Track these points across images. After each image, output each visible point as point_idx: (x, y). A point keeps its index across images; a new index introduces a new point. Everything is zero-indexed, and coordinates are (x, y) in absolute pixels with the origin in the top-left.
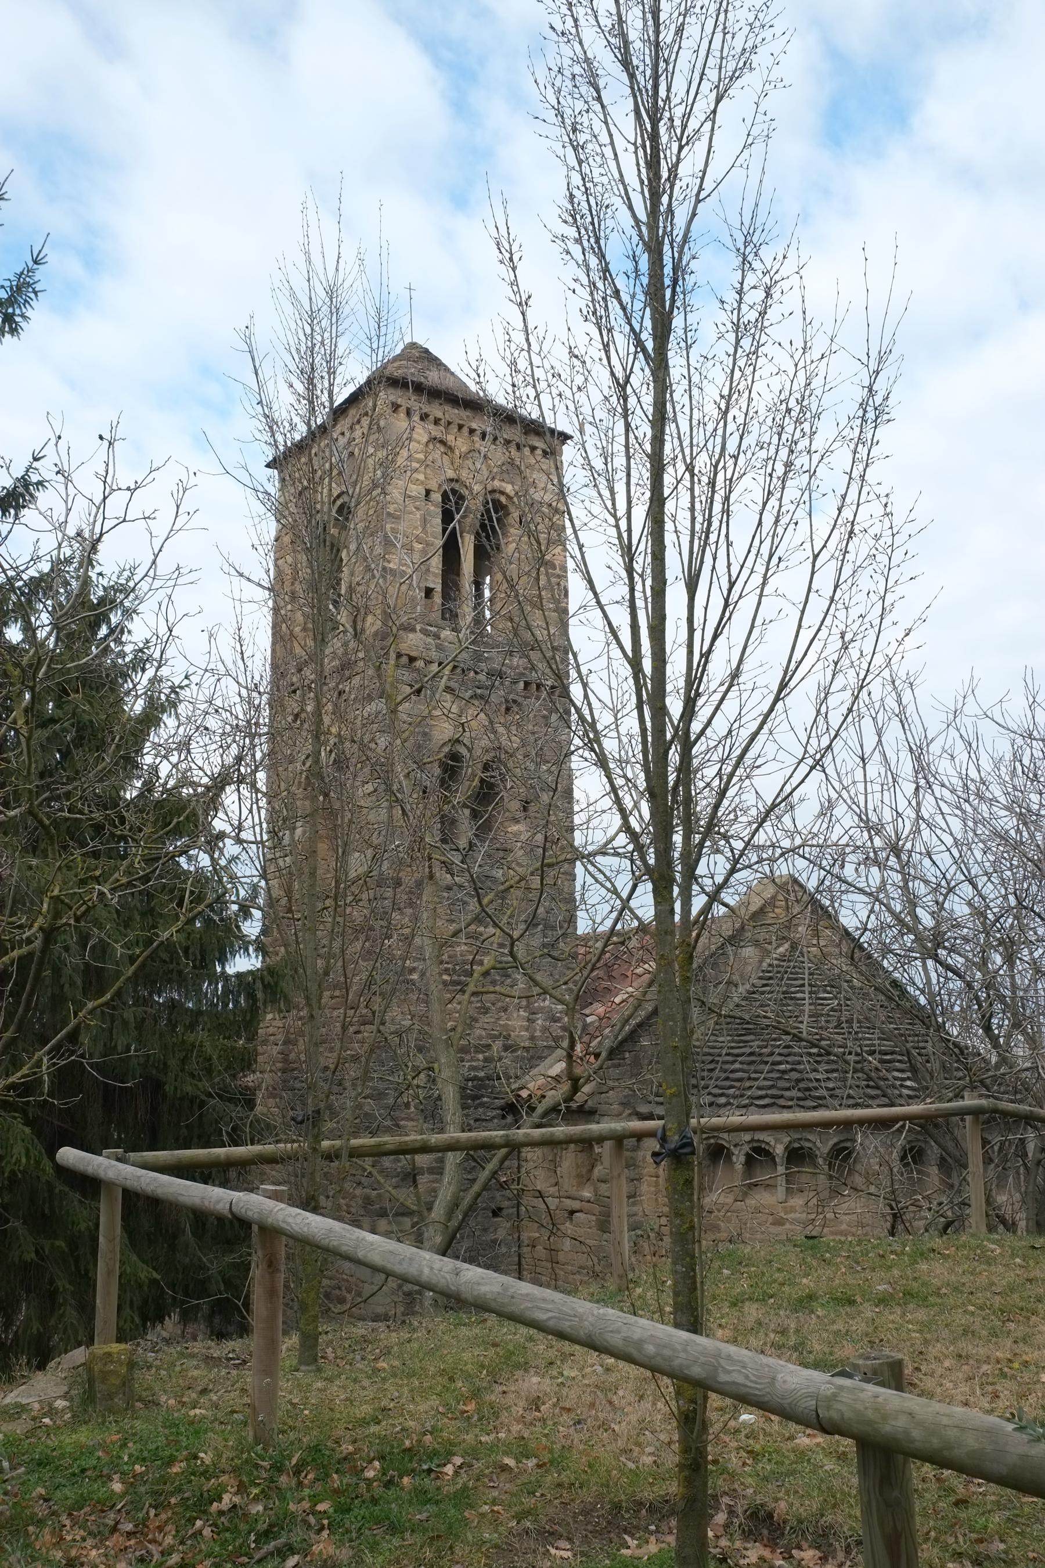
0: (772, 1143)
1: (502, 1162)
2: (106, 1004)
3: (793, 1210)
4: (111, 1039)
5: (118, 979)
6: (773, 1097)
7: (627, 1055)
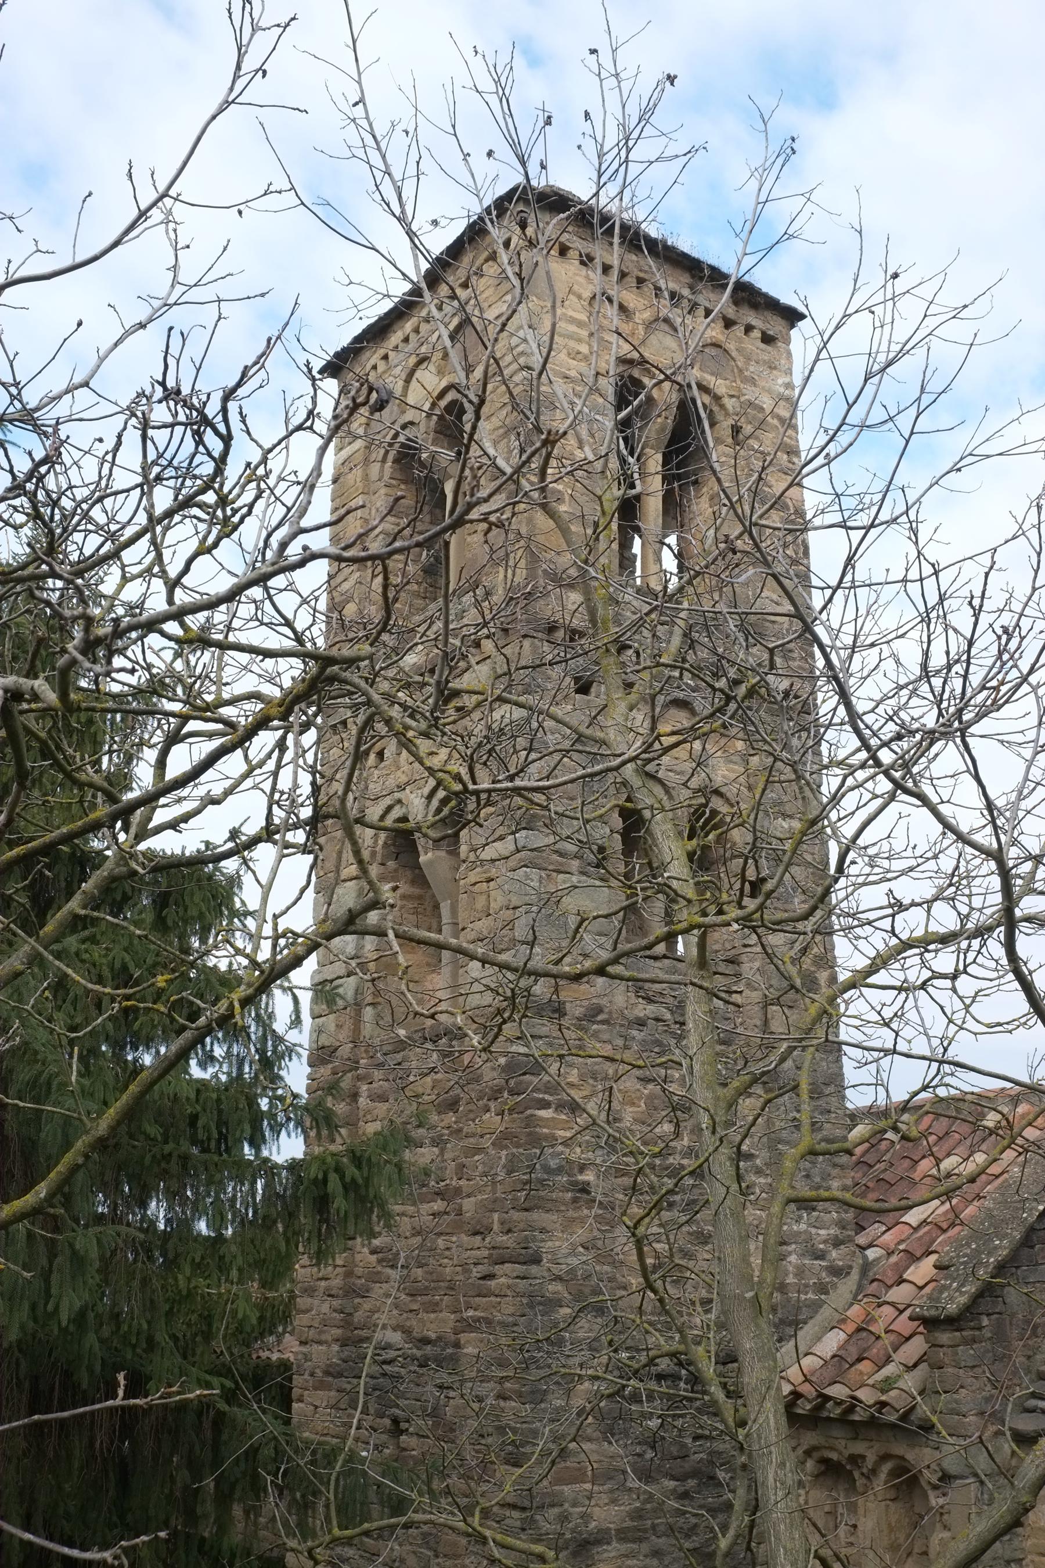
2: (34, 1213)
4: (48, 1295)
5: (67, 1146)
7: (985, 1321)
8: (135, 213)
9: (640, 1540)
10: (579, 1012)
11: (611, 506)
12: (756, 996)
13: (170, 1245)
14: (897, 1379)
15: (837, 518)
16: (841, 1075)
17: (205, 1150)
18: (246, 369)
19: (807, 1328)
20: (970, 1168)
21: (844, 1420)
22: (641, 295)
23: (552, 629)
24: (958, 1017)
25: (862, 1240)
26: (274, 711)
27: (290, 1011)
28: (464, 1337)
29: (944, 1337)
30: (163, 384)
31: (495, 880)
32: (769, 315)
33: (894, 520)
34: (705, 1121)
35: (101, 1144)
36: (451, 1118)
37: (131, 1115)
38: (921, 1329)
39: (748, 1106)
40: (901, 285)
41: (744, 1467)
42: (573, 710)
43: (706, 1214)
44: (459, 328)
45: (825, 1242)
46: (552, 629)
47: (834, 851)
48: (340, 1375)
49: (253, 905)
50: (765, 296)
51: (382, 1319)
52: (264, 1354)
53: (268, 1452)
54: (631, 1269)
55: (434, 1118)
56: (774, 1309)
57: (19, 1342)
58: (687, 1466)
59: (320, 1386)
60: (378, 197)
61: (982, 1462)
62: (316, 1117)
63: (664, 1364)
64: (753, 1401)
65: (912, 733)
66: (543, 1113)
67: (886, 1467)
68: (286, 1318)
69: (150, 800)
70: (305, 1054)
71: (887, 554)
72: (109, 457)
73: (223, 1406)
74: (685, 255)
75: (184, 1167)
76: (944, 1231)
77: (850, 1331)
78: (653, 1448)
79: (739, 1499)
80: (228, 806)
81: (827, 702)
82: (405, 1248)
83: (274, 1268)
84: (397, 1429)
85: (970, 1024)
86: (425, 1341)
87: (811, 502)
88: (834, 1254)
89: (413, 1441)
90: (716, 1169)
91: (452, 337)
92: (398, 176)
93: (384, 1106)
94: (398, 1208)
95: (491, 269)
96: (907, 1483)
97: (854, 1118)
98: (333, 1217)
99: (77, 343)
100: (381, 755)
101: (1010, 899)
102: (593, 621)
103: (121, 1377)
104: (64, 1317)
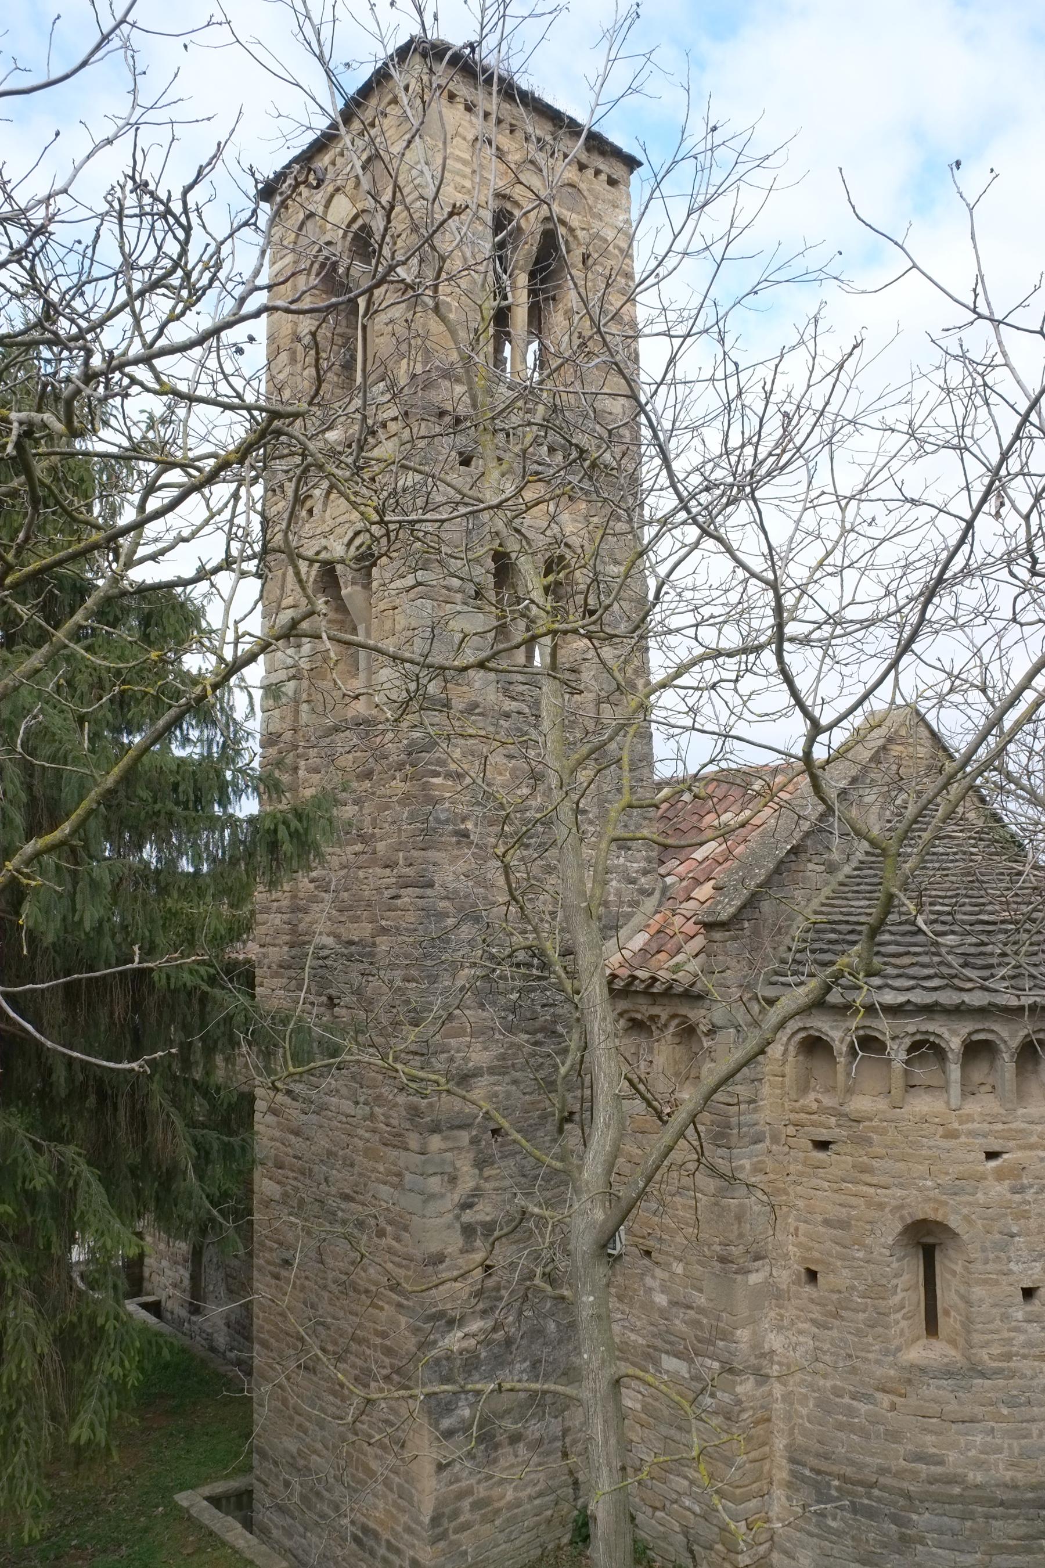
0: (946, 1036)
3: (970, 1118)
5: (82, 799)
7: (746, 924)
8: (99, 37)
10: (461, 706)
11: (489, 314)
12: (591, 696)
13: (162, 877)
14: (684, 965)
15: (663, 328)
16: (650, 754)
17: (186, 808)
18: (201, 169)
20: (742, 817)
21: (646, 993)
22: (513, 139)
23: (442, 414)
25: (662, 870)
26: (232, 457)
27: (246, 702)
28: (378, 940)
29: (718, 935)
30: (133, 178)
31: (398, 610)
32: (613, 161)
33: (706, 331)
34: (554, 782)
35: (111, 792)
36: (367, 784)
37: (129, 778)
39: (583, 776)
40: (718, 137)
41: (578, 1020)
42: (460, 477)
43: (554, 852)
44: (369, 160)
46: (442, 414)
47: (652, 583)
48: (289, 967)
49: (217, 625)
50: (611, 145)
51: (319, 928)
52: (234, 956)
53: (240, 1018)
54: (499, 888)
55: (355, 785)
56: (600, 919)
57: (54, 944)
59: (276, 975)
60: (300, 37)
61: (741, 1016)
62: (268, 786)
63: (521, 956)
64: (584, 977)
65: (717, 486)
66: (435, 780)
67: (676, 1021)
68: (249, 929)
69: (138, 526)
70: (258, 736)
71: (699, 358)
72: (90, 251)
73: (205, 987)
74: (549, 107)
75: (170, 820)
80: (191, 545)
81: (651, 468)
82: (335, 879)
83: (239, 895)
84: (331, 1003)
85: (747, 715)
86: (351, 943)
87: (641, 314)
89: (344, 1012)
90: (561, 817)
91: (364, 168)
92: (317, 21)
93: (318, 776)
94: (330, 850)
95: (393, 110)
96: (688, 1032)
97: (659, 786)
98: (281, 856)
99: (53, 158)
100: (310, 512)
101: (780, 626)
102: (474, 406)
103: (136, 948)
104: (87, 925)
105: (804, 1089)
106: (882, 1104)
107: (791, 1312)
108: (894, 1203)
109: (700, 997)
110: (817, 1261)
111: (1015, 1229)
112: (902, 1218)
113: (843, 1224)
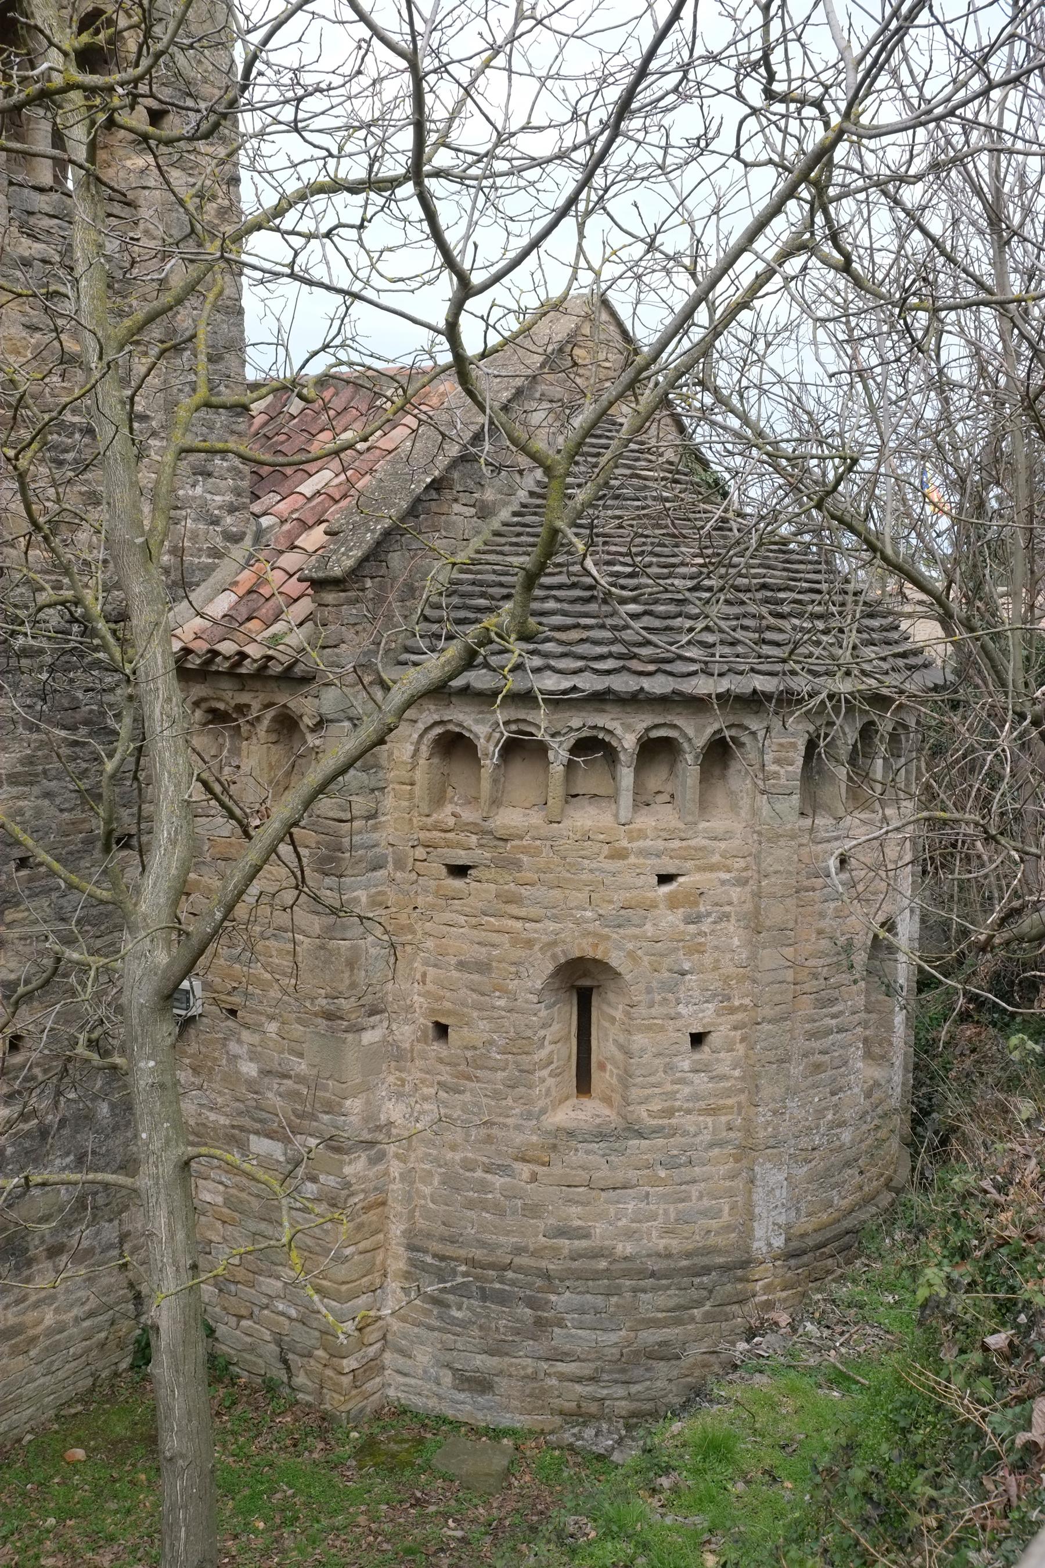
0: (619, 732)
1: (309, 802)
3: (642, 834)
6: (620, 657)
7: (369, 583)
9: (31, 784)
19: (199, 590)
21: (231, 673)
24: (363, 274)
25: (256, 508)
29: (330, 597)
38: (310, 591)
45: (220, 508)
47: (239, 54)
58: (79, 716)
76: (337, 502)
77: (241, 593)
78: (44, 700)
79: (125, 728)
85: (375, 277)
88: (229, 520)
96: (287, 725)
105: (439, 799)
106: (536, 818)
107: (415, 1075)
108: (545, 939)
109: (307, 679)
110: (449, 1013)
111: (687, 966)
112: (554, 957)
113: (483, 967)
